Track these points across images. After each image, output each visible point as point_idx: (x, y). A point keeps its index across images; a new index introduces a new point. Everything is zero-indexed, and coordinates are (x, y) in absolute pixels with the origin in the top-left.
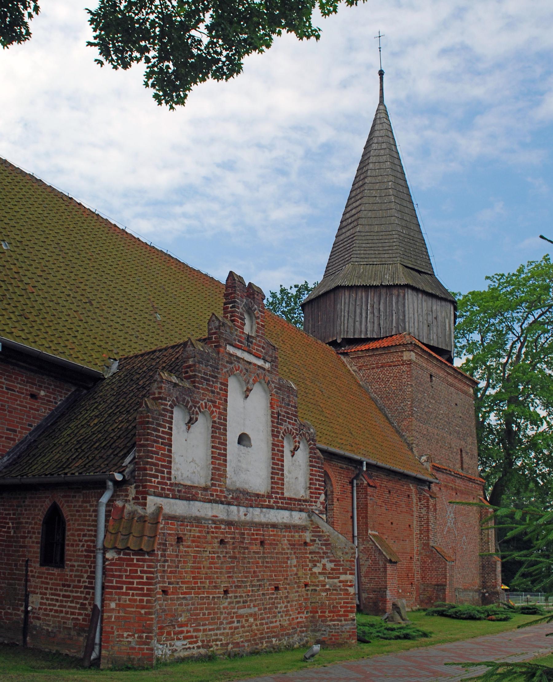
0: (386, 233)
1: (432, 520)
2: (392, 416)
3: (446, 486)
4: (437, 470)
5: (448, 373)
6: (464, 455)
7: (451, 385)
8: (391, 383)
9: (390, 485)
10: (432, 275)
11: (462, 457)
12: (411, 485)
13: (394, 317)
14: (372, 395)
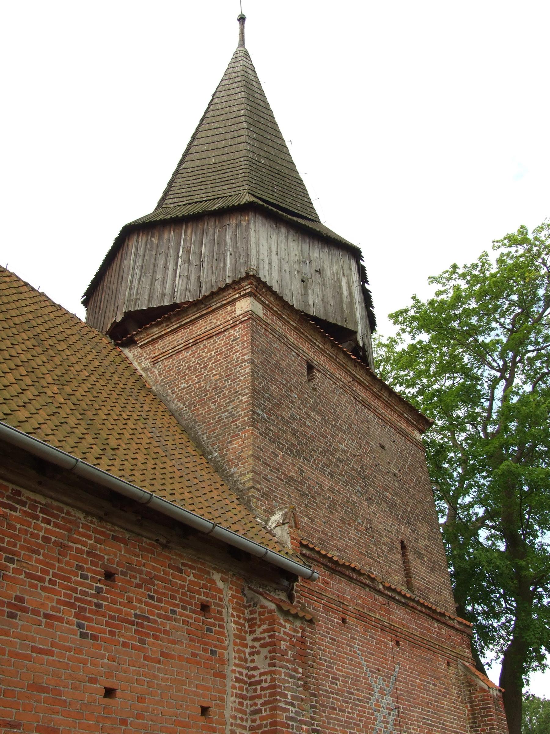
0: (228, 163)
1: (290, 690)
2: (209, 438)
3: (361, 617)
4: (333, 571)
5: (355, 379)
6: (411, 557)
7: (366, 405)
8: (212, 369)
9: (115, 554)
10: (319, 222)
11: (406, 563)
12: (217, 577)
13: (228, 261)
14: (173, 406)
